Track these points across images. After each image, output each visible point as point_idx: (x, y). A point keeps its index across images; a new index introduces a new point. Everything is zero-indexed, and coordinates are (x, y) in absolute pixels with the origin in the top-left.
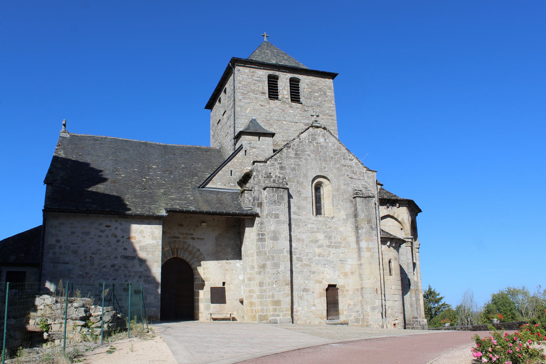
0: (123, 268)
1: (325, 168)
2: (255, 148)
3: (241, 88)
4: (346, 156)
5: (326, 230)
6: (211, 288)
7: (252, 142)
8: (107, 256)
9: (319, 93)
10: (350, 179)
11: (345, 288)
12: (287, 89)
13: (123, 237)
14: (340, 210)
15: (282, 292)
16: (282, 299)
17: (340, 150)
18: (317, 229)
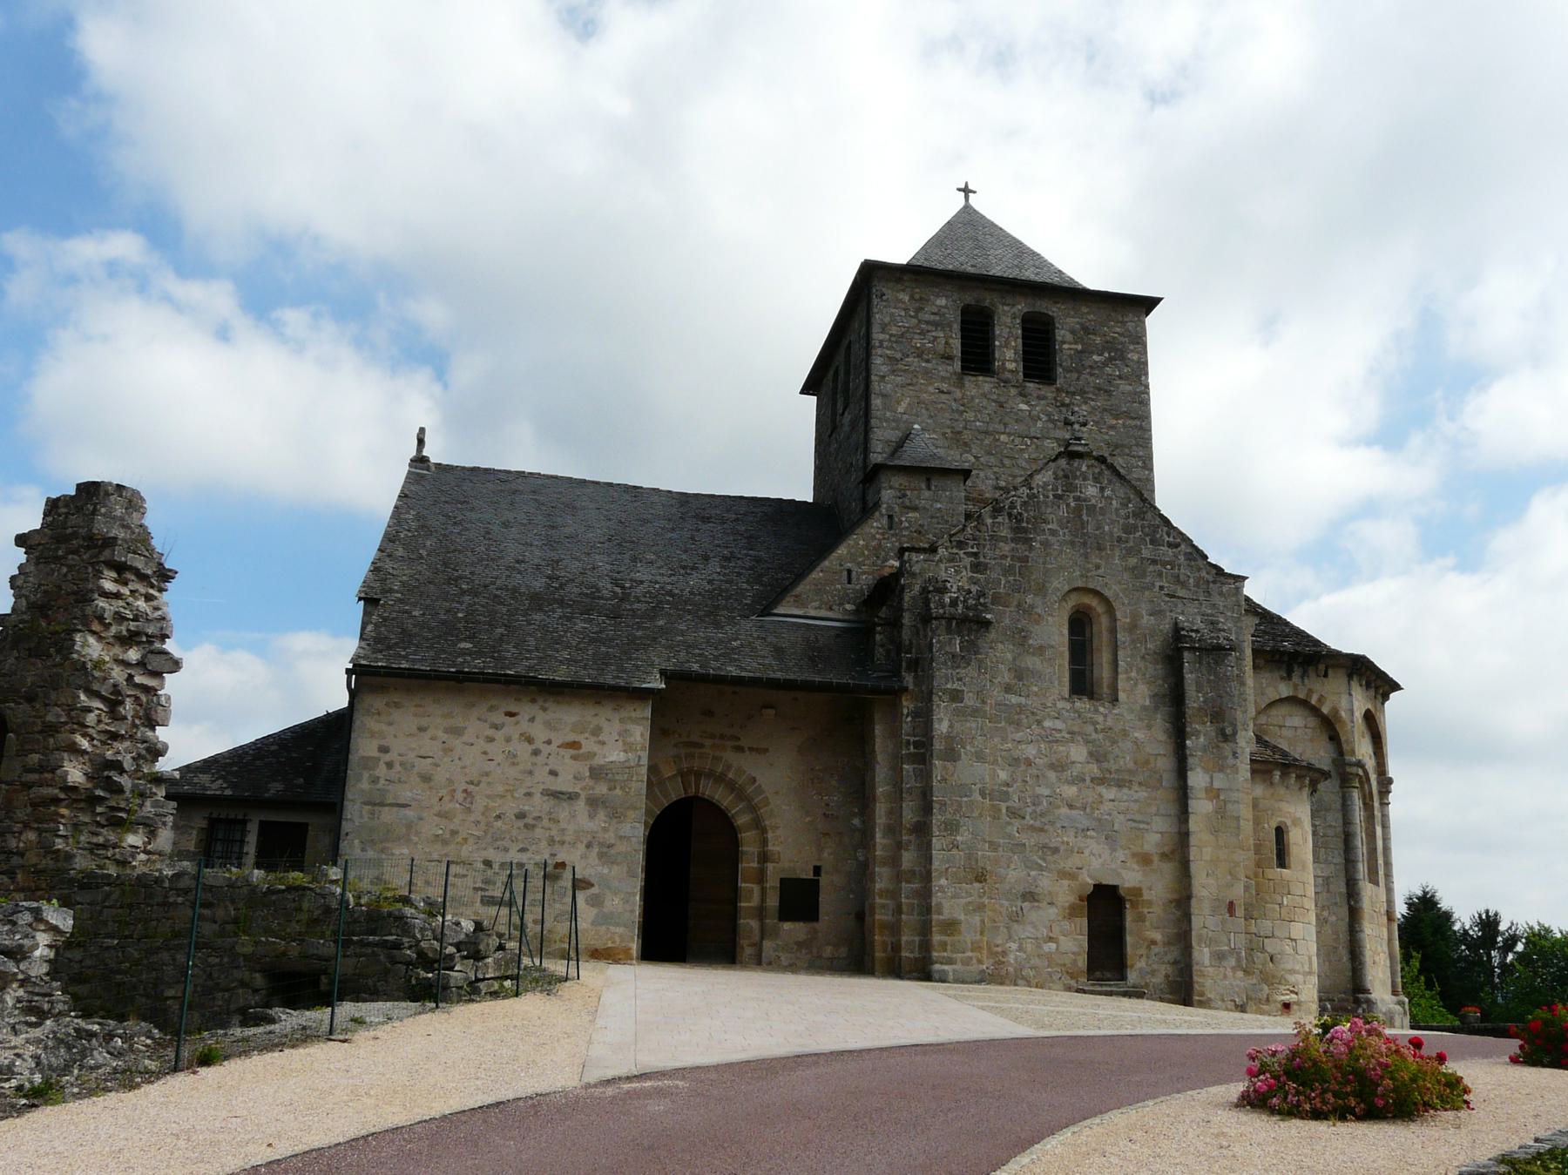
0: (545, 822)
1: (1098, 567)
2: (915, 509)
3: (885, 344)
4: (1158, 536)
5: (1094, 736)
6: (782, 880)
7: (908, 493)
8: (507, 791)
9: (1106, 355)
10: (1167, 599)
11: (1141, 895)
12: (1013, 344)
13: (549, 742)
14: (1136, 685)
15: (962, 897)
16: (962, 917)
17: (1143, 519)
18: (1069, 733)
